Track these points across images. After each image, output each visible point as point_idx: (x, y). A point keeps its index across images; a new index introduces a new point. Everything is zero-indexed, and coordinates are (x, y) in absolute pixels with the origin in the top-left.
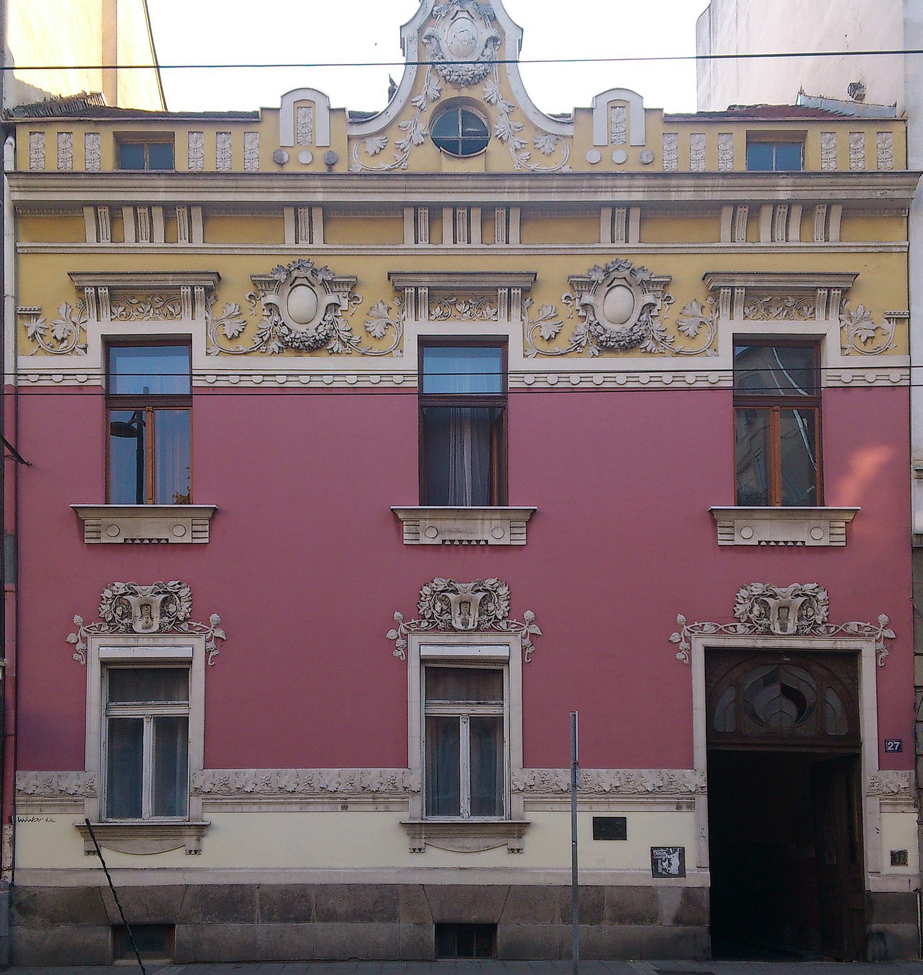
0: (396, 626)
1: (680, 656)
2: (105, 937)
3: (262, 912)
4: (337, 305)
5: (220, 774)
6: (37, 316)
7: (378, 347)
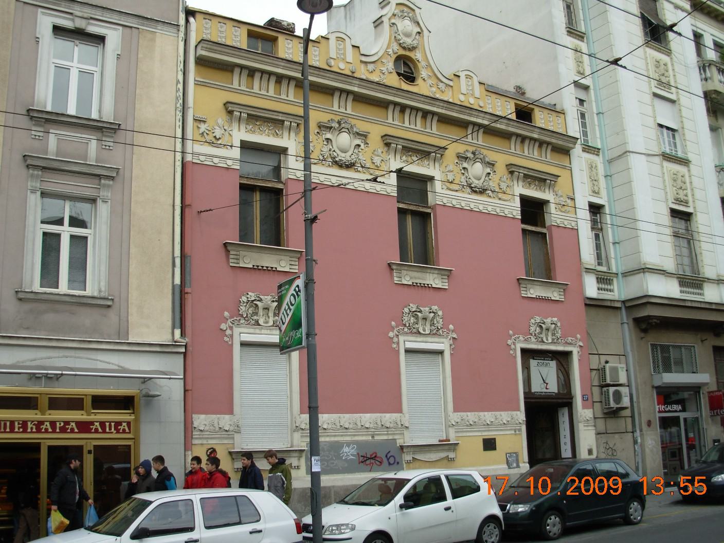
4: (359, 146)
6: (204, 122)
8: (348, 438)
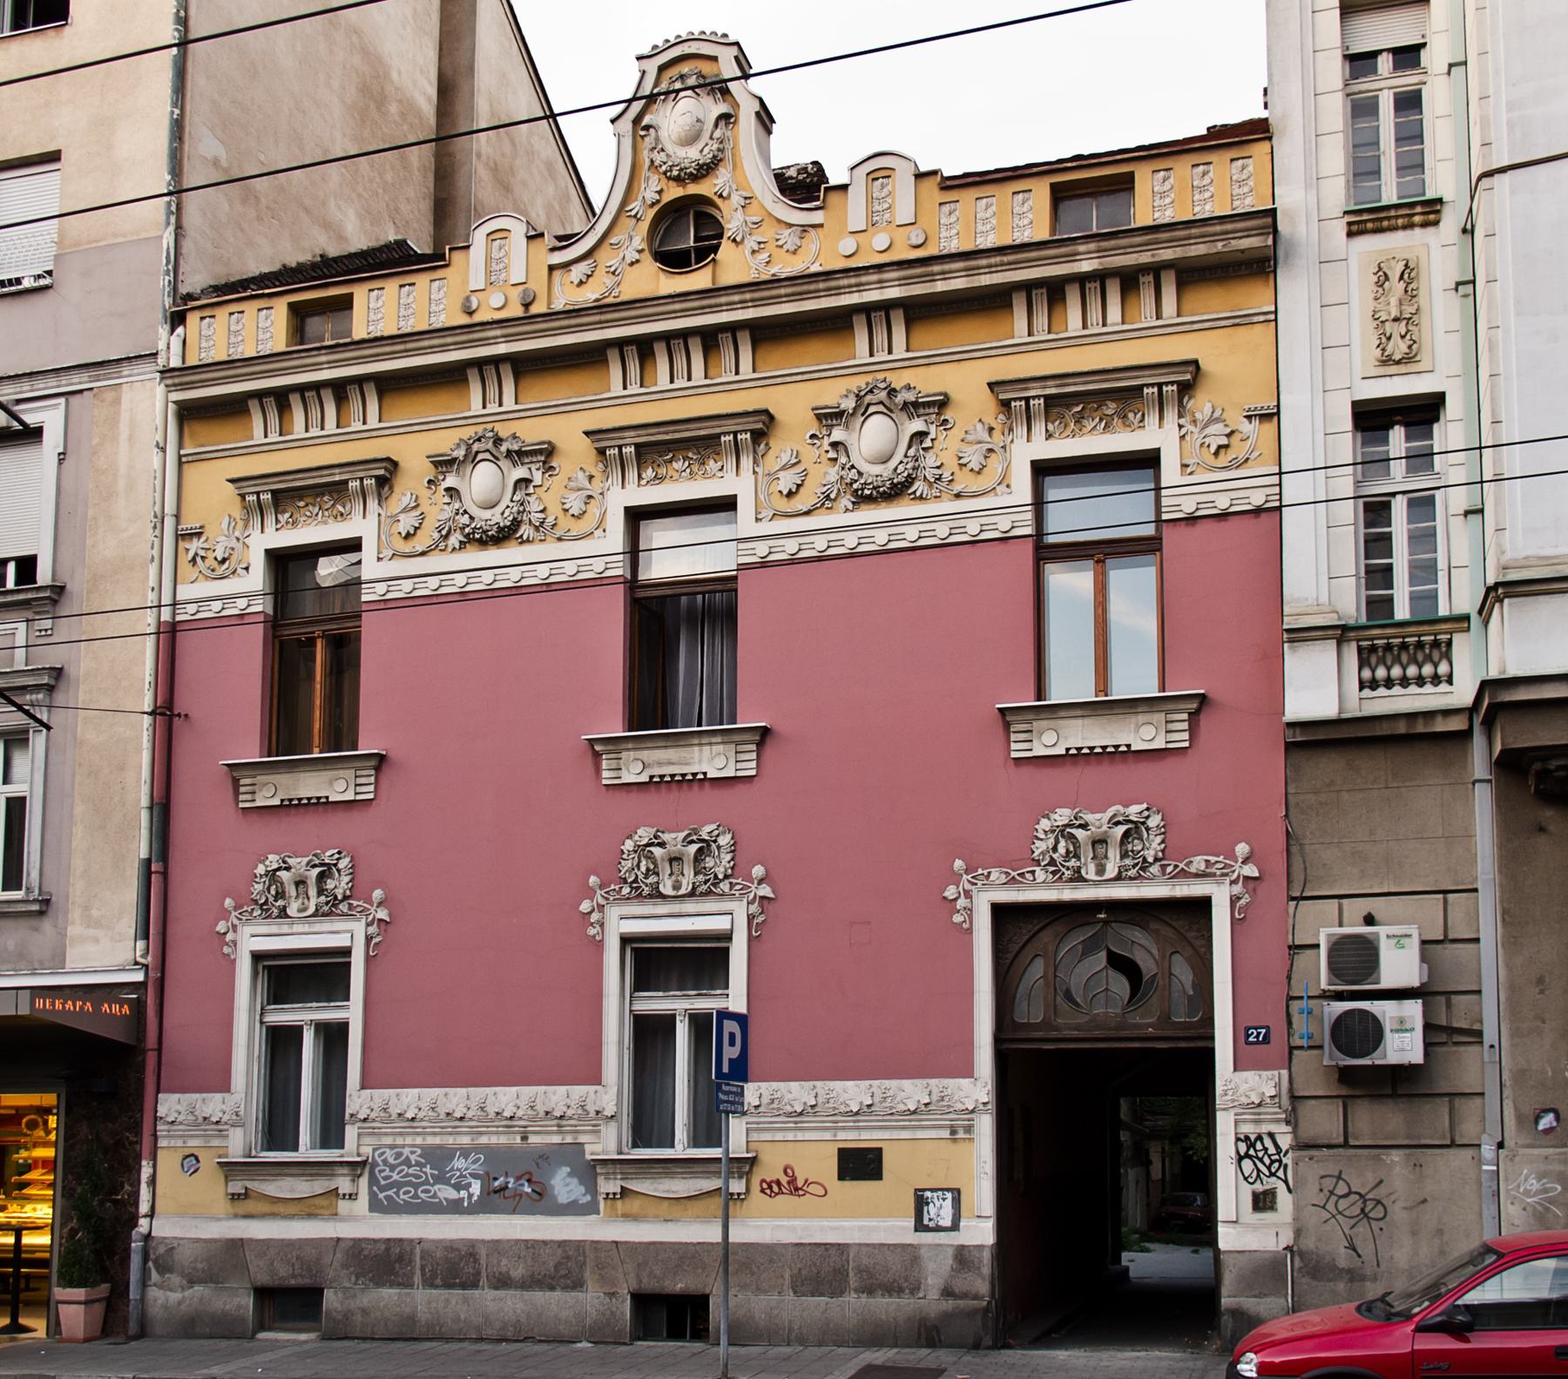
0: (590, 894)
1: (957, 918)
2: (248, 1302)
3: (423, 1274)
4: (527, 481)
5: (381, 1095)
6: (199, 535)
7: (578, 528)
8: (466, 1140)
